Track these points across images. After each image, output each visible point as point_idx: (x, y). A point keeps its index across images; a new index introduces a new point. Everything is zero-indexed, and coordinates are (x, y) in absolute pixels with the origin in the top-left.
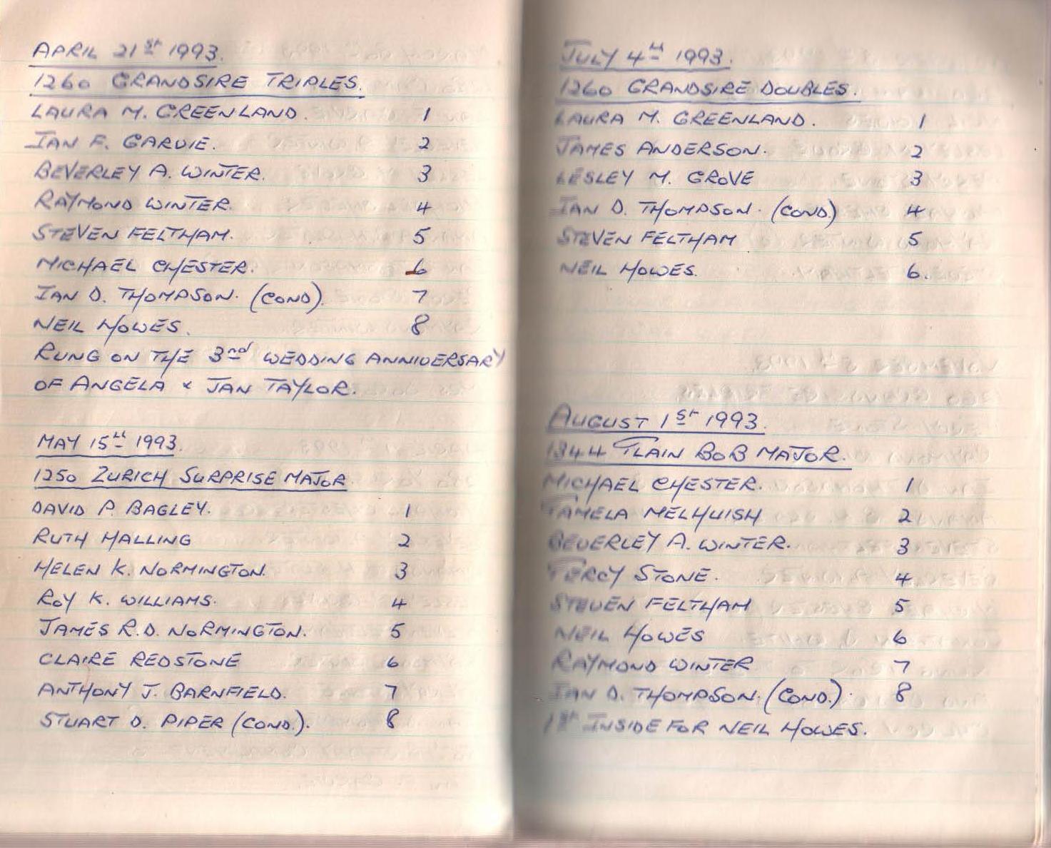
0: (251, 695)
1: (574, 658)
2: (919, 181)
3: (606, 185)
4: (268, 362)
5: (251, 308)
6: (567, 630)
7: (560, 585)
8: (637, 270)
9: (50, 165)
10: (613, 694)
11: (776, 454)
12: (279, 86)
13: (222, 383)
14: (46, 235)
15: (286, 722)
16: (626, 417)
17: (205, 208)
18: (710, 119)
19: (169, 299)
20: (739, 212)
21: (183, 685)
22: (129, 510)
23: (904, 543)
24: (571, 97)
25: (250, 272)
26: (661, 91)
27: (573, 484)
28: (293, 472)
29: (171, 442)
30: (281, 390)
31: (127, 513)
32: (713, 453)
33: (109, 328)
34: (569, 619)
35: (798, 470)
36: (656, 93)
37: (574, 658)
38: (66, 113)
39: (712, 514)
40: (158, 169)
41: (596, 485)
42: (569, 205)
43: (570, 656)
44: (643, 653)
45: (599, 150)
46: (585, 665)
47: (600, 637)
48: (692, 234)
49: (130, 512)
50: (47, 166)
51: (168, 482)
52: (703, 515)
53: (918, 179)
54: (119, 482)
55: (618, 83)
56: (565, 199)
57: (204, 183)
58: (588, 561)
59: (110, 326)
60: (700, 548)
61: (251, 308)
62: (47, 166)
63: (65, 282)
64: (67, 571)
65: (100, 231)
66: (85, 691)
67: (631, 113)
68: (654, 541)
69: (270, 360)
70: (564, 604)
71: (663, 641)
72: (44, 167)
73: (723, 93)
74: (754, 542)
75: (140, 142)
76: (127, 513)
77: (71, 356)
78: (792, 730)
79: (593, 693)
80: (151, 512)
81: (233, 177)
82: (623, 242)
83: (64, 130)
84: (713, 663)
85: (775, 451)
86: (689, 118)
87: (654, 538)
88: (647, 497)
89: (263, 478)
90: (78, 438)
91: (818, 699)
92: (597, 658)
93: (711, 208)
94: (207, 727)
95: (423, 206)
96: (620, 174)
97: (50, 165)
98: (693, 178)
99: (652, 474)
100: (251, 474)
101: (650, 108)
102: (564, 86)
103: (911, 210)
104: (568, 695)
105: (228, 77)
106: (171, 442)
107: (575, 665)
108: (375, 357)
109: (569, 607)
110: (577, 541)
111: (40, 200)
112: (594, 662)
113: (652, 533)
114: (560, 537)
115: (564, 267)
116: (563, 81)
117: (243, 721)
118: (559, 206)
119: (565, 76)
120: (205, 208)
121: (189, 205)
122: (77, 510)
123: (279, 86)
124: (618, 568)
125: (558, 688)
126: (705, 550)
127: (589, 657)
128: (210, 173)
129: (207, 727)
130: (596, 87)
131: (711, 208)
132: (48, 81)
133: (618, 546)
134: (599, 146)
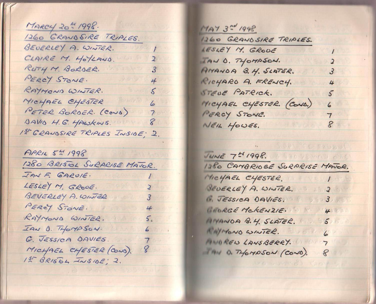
0: (231, 105)
5: (108, 253)
7: (204, 109)
12: (110, 38)
13: (30, 227)
14: (242, 115)
15: (120, 112)
17: (284, 72)
19: (257, 73)
20: (274, 83)
23: (74, 229)
24: (206, 42)
27: (215, 178)
28: (122, 133)
29: (328, 199)
32: (65, 112)
36: (238, 42)
39: (52, 48)
42: (207, 60)
50: (29, 46)
53: (53, 164)
55: (224, 38)
56: (205, 58)
57: (301, 247)
60: (327, 242)
61: (108, 253)
62: (29, 46)
63: (35, 85)
72: (27, 46)
78: (55, 123)
80: (67, 177)
86: (255, 50)
101: (241, 47)
106: (328, 199)
109: (208, 94)
115: (205, 124)
116: (202, 38)
117: (111, 250)
118: (203, 60)
119: (202, 36)
120: (284, 72)
122: (134, 134)
123: (110, 38)
124: (288, 240)
126: (248, 233)
128: (257, 232)
132: (28, 164)
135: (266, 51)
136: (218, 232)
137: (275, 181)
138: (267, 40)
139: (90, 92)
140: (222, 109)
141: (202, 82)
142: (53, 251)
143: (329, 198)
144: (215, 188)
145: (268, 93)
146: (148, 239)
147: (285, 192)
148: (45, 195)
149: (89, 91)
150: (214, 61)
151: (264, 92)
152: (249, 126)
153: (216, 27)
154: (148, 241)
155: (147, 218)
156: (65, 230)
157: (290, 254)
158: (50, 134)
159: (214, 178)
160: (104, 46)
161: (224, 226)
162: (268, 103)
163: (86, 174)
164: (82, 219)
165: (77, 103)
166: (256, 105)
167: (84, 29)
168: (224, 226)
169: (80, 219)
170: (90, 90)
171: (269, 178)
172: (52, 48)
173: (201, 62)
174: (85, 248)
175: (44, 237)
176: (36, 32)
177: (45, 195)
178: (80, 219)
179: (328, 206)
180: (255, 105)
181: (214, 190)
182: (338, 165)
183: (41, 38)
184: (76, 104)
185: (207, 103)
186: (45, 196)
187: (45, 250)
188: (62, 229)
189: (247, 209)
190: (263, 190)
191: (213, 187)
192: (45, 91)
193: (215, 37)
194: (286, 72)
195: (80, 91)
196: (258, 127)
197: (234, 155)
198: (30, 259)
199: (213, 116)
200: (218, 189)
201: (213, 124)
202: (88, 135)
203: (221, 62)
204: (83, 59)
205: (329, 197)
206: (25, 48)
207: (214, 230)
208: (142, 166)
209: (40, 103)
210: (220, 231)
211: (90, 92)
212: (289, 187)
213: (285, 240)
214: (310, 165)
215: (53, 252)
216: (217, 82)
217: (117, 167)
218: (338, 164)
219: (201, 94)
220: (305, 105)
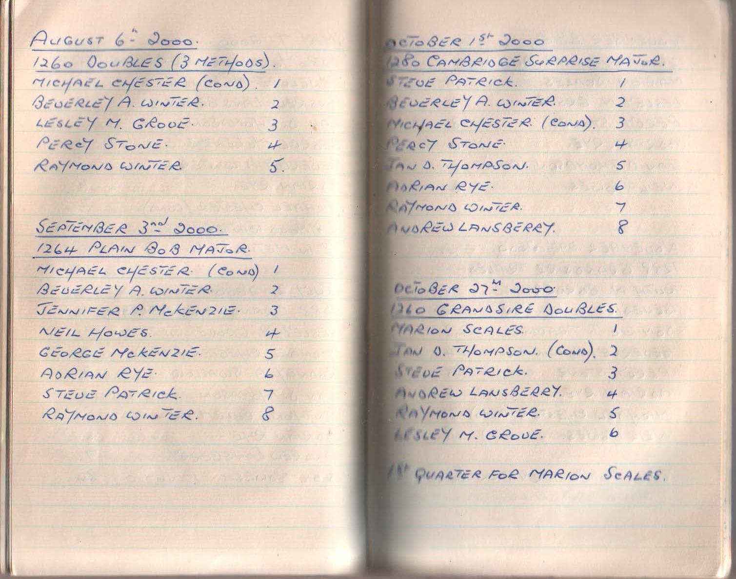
1: (409, 411)
4: (124, 169)
8: (103, 333)
11: (620, 61)
22: (39, 291)
26: (50, 169)
30: (208, 252)
31: (38, 293)
33: (556, 389)
37: (409, 411)
38: (568, 311)
45: (440, 415)
49: (39, 293)
50: (41, 99)
51: (128, 232)
52: (72, 272)
54: (573, 314)
66: (69, 273)
68: (556, 392)
70: (405, 373)
71: (194, 315)
75: (144, 124)
76: (38, 293)
77: (141, 167)
82: (164, 355)
85: (619, 58)
87: (556, 390)
90: (95, 120)
91: (489, 64)
92: (428, 409)
94: (177, 170)
95: (612, 393)
96: (113, 287)
97: (132, 59)
99: (463, 324)
102: (393, 309)
103: (68, 271)
104: (398, 166)
111: (40, 165)
113: (555, 386)
121: (171, 103)
129: (177, 170)
130: (61, 62)
131: (494, 164)
134: (440, 412)
137: (526, 418)
138: (518, 309)
139: (159, 168)
142: (85, 273)
143: (622, 120)
144: (419, 372)
145: (522, 370)
147: (541, 397)
148: (71, 393)
150: (409, 167)
151: (513, 370)
153: (554, 387)
156: (479, 126)
159: (403, 126)
161: (437, 404)
163: (148, 61)
167: (199, 254)
168: (437, 404)
170: (159, 164)
172: (68, 125)
173: (393, 65)
175: (515, 410)
176: (56, 54)
177: (71, 393)
179: (614, 386)
181: (417, 377)
182: (642, 59)
183: (68, 65)
184: (65, 86)
186: (71, 394)
189: (478, 165)
190: (468, 211)
192: (115, 122)
194: (80, 291)
200: (426, 374)
203: (420, 168)
204: (236, 62)
205: (624, 119)
208: (431, 330)
209: (56, 419)
211: (159, 168)
213: (423, 372)
214: (587, 58)
218: (641, 55)
219: (396, 374)
220: (584, 352)
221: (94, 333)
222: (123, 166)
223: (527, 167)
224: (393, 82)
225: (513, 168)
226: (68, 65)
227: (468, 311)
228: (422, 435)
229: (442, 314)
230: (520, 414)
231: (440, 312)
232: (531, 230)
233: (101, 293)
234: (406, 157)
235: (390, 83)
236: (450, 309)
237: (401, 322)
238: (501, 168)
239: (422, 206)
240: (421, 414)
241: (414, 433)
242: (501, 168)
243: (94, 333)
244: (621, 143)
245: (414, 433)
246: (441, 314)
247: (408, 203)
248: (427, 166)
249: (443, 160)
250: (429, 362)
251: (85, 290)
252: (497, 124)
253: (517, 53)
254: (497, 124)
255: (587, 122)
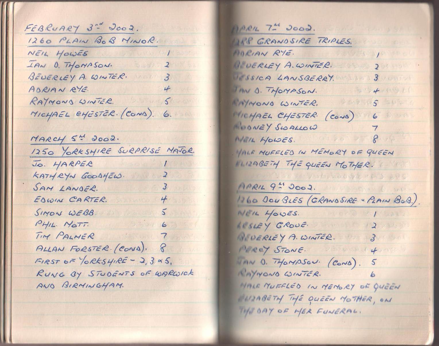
2: (168, 78)
3: (258, 229)
4: (93, 79)
6: (240, 138)
7: (240, 244)
9: (34, 75)
10: (259, 311)
16: (281, 102)
18: (287, 152)
21: (41, 221)
25: (116, 115)
27: (244, 116)
34: (241, 146)
35: (341, 48)
40: (55, 114)
41: (253, 116)
43: (246, 271)
44: (275, 219)
46: (250, 275)
47: (252, 141)
48: (278, 296)
58: (252, 51)
59: (283, 51)
64: (290, 202)
65: (309, 102)
67: (261, 211)
69: (94, 78)
73: (82, 251)
74: (307, 273)
75: (282, 225)
79: (254, 262)
81: (112, 78)
83: (41, 60)
84: (303, 273)
88: (275, 121)
89: (155, 151)
93: (297, 90)
97: (34, 75)
98: (278, 226)
100: (308, 67)
105: (33, 74)
107: (247, 275)
108: (43, 188)
110: (245, 297)
111: (32, 101)
112: (254, 274)
114: (238, 63)
115: (242, 284)
125: (236, 88)
127: (252, 272)
131: (297, 90)
133: (289, 225)
135: (298, 29)
136: (252, 274)
140: (260, 244)
141: (239, 274)
146: (165, 234)
149: (284, 251)
152: (288, 215)
154: (165, 236)
155: (166, 101)
157: (338, 264)
158: (62, 102)
160: (126, 257)
162: (306, 114)
164: (91, 102)
165: (72, 66)
166: (292, 117)
169: (90, 102)
171: (94, 249)
174: (81, 211)
178: (90, 102)
180: (291, 117)
185: (239, 114)
187: (60, 139)
188: (70, 66)
191: (246, 236)
193: (254, 209)
195: (102, 77)
196: (299, 215)
197: (376, 127)
198: (373, 263)
199: (250, 252)
200: (248, 66)
201: (248, 211)
202: (103, 153)
206: (71, 275)
207: (240, 100)
210: (247, 103)
212: (337, 261)
215: (262, 117)
216: (251, 115)
217: (155, 153)
221: (268, 214)
222: (93, 78)
223: (319, 262)
224: (252, 313)
225: (308, 92)
226: (48, 42)
227: (327, 202)
228: (253, 226)
229: (260, 44)
230: (320, 152)
231: (259, 43)
232: (321, 80)
233: (64, 79)
234: (245, 84)
235: (237, 52)
236: (264, 41)
237: (242, 209)
238: (306, 263)
239: (253, 102)
240: (245, 104)
241: (248, 225)
242: (306, 263)
243: (268, 214)
244: (373, 250)
245: (248, 225)
246: (259, 44)
247: (264, 247)
248: (257, 91)
249: (290, 295)
250: (254, 98)
251: (312, 115)
252: (301, 201)
253: (309, 36)
254: (301, 201)
255: (353, 262)
